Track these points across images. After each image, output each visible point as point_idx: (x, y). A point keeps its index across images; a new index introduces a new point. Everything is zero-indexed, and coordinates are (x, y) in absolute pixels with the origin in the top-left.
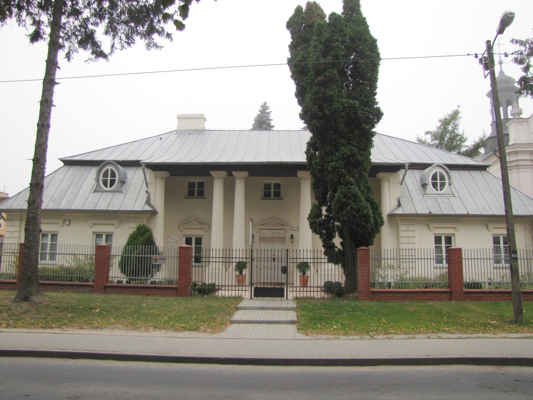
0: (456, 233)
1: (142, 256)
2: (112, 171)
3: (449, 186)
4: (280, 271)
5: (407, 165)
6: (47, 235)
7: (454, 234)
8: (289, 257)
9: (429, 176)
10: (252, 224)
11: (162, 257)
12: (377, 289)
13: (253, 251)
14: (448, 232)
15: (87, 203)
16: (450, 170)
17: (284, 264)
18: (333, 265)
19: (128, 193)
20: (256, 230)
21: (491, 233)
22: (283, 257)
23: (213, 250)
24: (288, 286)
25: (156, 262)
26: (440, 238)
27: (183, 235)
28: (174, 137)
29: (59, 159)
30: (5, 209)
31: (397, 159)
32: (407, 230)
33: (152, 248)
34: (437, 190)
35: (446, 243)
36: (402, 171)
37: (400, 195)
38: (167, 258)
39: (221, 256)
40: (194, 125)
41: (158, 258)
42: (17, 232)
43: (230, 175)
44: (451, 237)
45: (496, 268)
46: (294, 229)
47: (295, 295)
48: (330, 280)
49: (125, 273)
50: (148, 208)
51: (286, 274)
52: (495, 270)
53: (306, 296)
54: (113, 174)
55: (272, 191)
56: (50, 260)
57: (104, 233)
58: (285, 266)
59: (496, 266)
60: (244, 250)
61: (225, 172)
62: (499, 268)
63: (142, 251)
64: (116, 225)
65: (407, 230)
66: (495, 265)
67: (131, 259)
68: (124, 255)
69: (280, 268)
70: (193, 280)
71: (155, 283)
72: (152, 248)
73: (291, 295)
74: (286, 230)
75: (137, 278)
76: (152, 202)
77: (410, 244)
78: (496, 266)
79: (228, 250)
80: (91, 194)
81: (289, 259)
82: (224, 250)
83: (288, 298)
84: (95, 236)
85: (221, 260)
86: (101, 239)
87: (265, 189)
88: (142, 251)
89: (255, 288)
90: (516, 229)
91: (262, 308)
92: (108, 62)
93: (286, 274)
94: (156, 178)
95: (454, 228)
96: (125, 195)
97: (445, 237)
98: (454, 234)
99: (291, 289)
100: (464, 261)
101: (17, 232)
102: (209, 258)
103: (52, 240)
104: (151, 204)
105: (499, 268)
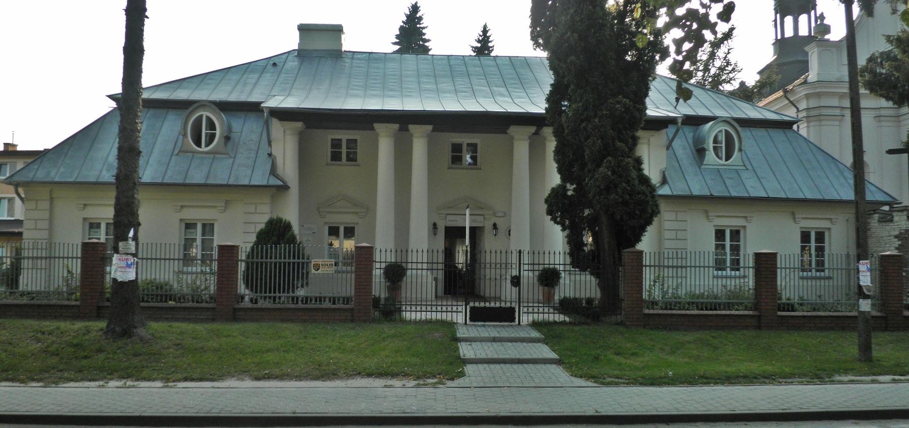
0: (834, 228)
1: (285, 260)
2: (208, 119)
3: (740, 153)
4: (509, 281)
5: (680, 121)
6: (196, 224)
7: (744, 227)
8: (522, 262)
9: (709, 137)
11: (327, 263)
13: (522, 254)
14: (736, 223)
15: (169, 173)
16: (741, 126)
17: (515, 273)
19: (239, 156)
20: (441, 215)
21: (713, 224)
22: (514, 261)
23: (412, 252)
24: (521, 305)
25: (318, 269)
27: (325, 223)
28: (293, 63)
29: (108, 96)
31: (658, 108)
34: (720, 158)
36: (671, 130)
39: (425, 260)
40: (321, 43)
41: (321, 263)
42: (45, 219)
43: (404, 129)
45: (717, 277)
46: (499, 214)
47: (531, 318)
50: (274, 181)
51: (518, 288)
53: (419, 318)
54: (211, 125)
55: (344, 150)
57: (200, 220)
58: (516, 276)
60: (393, 251)
61: (301, 123)
62: (722, 277)
63: (280, 254)
64: (362, 214)
65: (674, 219)
67: (266, 267)
68: (250, 260)
69: (509, 278)
70: (374, 294)
73: (526, 319)
74: (486, 216)
75: (263, 294)
76: (280, 171)
79: (504, 252)
80: (174, 158)
81: (522, 265)
82: (430, 251)
83: (521, 323)
84: (183, 226)
85: (425, 266)
86: (98, 230)
87: (453, 152)
88: (280, 254)
89: (471, 308)
90: (836, 220)
91: (494, 340)
93: (518, 288)
94: (284, 132)
95: (746, 217)
96: (233, 159)
99: (525, 310)
100: (779, 271)
101: (45, 219)
102: (407, 263)
103: (203, 234)
104: (278, 175)
105: (722, 277)
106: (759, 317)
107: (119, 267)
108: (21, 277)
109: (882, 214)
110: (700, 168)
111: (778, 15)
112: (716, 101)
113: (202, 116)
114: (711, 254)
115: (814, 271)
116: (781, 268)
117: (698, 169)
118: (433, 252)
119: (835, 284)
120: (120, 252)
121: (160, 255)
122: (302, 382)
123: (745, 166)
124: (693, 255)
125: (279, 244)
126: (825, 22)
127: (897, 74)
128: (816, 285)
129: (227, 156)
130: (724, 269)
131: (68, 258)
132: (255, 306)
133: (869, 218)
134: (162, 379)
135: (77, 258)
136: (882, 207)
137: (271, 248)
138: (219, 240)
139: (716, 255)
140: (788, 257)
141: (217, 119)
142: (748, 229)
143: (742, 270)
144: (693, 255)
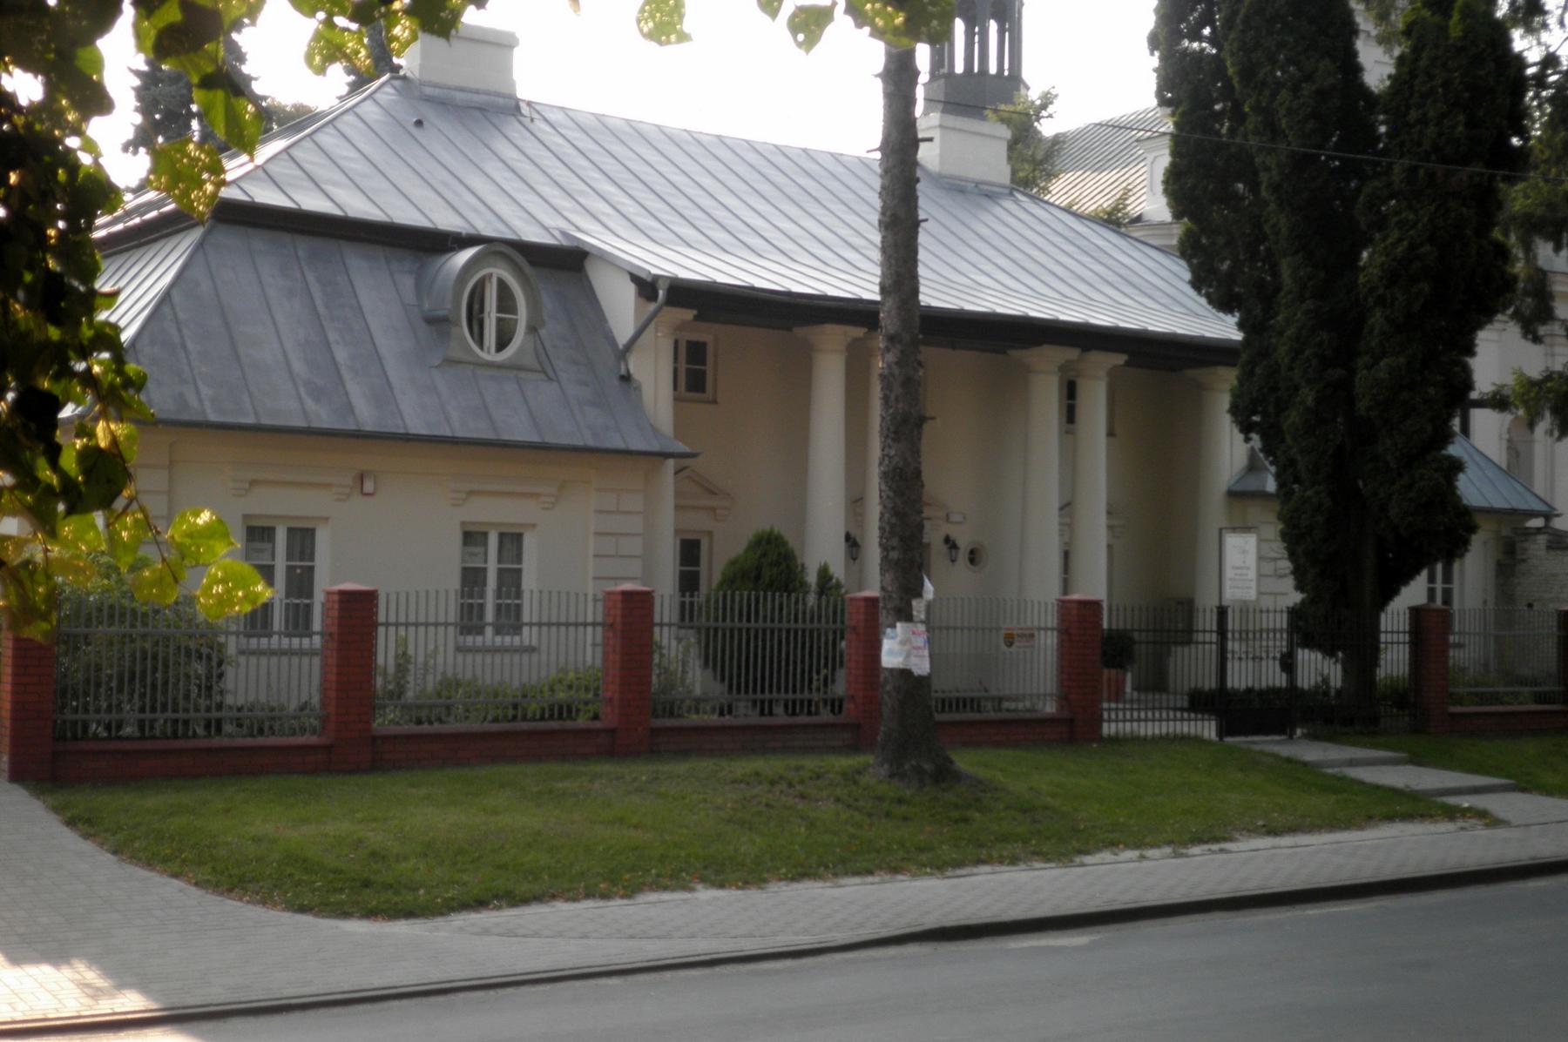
1: (773, 625)
2: (502, 285)
12: (233, 736)
18: (1320, 656)
33: (729, 598)
38: (1036, 633)
48: (1200, 685)
49: (723, 679)
52: (460, 657)
54: (506, 301)
56: (461, 634)
59: (301, 644)
66: (461, 639)
71: (261, 731)
72: (729, 598)
78: (301, 644)
86: (268, 546)
92: (1054, 92)
106: (1072, 721)
107: (914, 648)
108: (1172, 660)
112: (479, 198)
113: (491, 275)
114: (452, 597)
115: (489, 631)
116: (387, 625)
118: (1398, 614)
119: (1467, 656)
120: (915, 619)
121: (407, 616)
122: (1438, 825)
124: (555, 599)
125: (756, 590)
126: (867, 29)
128: (521, 664)
130: (480, 631)
131: (407, 625)
132: (727, 720)
133: (1527, 540)
134: (1169, 843)
135: (387, 625)
136: (1527, 520)
137: (765, 598)
138: (329, 579)
139: (462, 597)
140: (432, 596)
141: (472, 276)
143: (526, 630)
144: (555, 599)
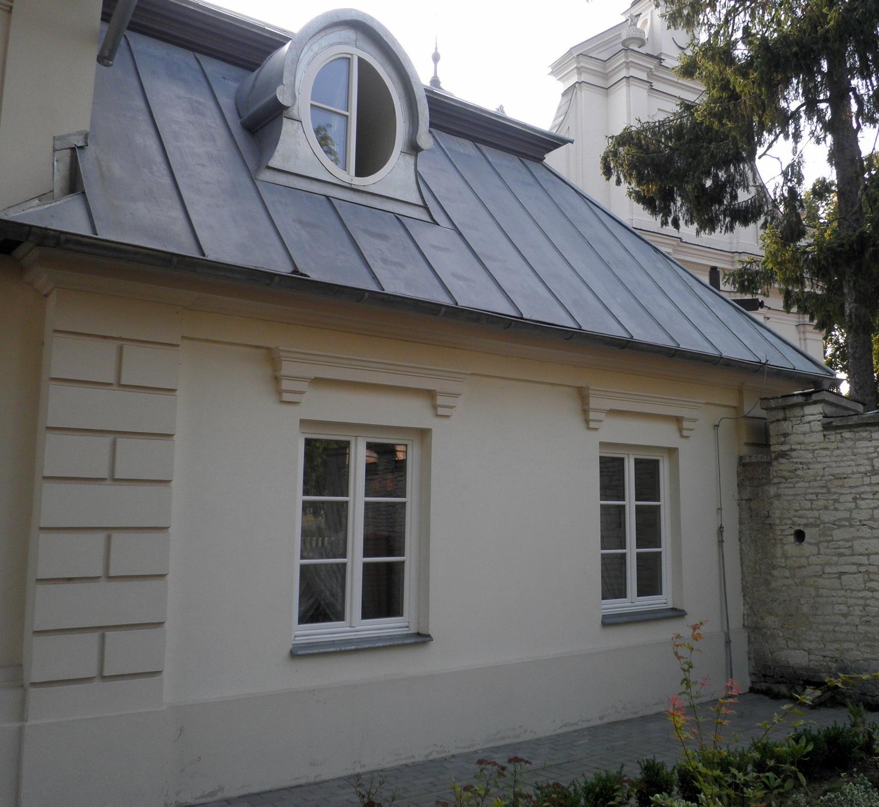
3: (410, 160)
7: (424, 434)
10: (624, 218)
21: (297, 413)
26: (341, 449)
30: (601, 477)
32: (110, 378)
35: (345, 505)
37: (86, 127)
44: (657, 461)
65: (110, 378)
77: (114, 585)
95: (430, 394)
97: (638, 462)
98: (424, 434)
109: (832, 404)
110: (253, 180)
111: (347, 463)
117: (245, 180)
123: (425, 207)
127: (642, 155)
129: (836, 476)
142: (436, 440)
